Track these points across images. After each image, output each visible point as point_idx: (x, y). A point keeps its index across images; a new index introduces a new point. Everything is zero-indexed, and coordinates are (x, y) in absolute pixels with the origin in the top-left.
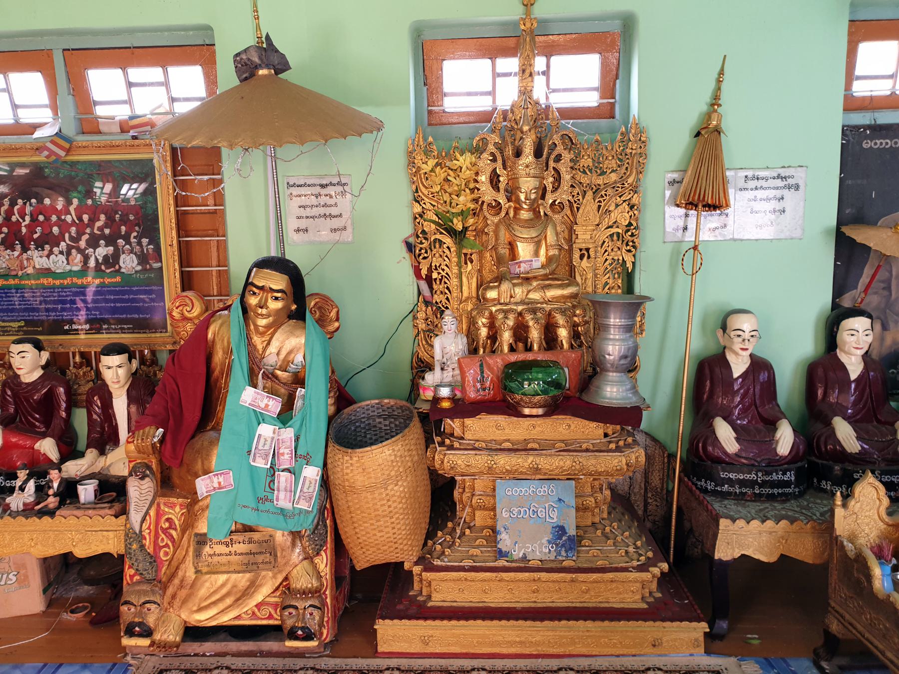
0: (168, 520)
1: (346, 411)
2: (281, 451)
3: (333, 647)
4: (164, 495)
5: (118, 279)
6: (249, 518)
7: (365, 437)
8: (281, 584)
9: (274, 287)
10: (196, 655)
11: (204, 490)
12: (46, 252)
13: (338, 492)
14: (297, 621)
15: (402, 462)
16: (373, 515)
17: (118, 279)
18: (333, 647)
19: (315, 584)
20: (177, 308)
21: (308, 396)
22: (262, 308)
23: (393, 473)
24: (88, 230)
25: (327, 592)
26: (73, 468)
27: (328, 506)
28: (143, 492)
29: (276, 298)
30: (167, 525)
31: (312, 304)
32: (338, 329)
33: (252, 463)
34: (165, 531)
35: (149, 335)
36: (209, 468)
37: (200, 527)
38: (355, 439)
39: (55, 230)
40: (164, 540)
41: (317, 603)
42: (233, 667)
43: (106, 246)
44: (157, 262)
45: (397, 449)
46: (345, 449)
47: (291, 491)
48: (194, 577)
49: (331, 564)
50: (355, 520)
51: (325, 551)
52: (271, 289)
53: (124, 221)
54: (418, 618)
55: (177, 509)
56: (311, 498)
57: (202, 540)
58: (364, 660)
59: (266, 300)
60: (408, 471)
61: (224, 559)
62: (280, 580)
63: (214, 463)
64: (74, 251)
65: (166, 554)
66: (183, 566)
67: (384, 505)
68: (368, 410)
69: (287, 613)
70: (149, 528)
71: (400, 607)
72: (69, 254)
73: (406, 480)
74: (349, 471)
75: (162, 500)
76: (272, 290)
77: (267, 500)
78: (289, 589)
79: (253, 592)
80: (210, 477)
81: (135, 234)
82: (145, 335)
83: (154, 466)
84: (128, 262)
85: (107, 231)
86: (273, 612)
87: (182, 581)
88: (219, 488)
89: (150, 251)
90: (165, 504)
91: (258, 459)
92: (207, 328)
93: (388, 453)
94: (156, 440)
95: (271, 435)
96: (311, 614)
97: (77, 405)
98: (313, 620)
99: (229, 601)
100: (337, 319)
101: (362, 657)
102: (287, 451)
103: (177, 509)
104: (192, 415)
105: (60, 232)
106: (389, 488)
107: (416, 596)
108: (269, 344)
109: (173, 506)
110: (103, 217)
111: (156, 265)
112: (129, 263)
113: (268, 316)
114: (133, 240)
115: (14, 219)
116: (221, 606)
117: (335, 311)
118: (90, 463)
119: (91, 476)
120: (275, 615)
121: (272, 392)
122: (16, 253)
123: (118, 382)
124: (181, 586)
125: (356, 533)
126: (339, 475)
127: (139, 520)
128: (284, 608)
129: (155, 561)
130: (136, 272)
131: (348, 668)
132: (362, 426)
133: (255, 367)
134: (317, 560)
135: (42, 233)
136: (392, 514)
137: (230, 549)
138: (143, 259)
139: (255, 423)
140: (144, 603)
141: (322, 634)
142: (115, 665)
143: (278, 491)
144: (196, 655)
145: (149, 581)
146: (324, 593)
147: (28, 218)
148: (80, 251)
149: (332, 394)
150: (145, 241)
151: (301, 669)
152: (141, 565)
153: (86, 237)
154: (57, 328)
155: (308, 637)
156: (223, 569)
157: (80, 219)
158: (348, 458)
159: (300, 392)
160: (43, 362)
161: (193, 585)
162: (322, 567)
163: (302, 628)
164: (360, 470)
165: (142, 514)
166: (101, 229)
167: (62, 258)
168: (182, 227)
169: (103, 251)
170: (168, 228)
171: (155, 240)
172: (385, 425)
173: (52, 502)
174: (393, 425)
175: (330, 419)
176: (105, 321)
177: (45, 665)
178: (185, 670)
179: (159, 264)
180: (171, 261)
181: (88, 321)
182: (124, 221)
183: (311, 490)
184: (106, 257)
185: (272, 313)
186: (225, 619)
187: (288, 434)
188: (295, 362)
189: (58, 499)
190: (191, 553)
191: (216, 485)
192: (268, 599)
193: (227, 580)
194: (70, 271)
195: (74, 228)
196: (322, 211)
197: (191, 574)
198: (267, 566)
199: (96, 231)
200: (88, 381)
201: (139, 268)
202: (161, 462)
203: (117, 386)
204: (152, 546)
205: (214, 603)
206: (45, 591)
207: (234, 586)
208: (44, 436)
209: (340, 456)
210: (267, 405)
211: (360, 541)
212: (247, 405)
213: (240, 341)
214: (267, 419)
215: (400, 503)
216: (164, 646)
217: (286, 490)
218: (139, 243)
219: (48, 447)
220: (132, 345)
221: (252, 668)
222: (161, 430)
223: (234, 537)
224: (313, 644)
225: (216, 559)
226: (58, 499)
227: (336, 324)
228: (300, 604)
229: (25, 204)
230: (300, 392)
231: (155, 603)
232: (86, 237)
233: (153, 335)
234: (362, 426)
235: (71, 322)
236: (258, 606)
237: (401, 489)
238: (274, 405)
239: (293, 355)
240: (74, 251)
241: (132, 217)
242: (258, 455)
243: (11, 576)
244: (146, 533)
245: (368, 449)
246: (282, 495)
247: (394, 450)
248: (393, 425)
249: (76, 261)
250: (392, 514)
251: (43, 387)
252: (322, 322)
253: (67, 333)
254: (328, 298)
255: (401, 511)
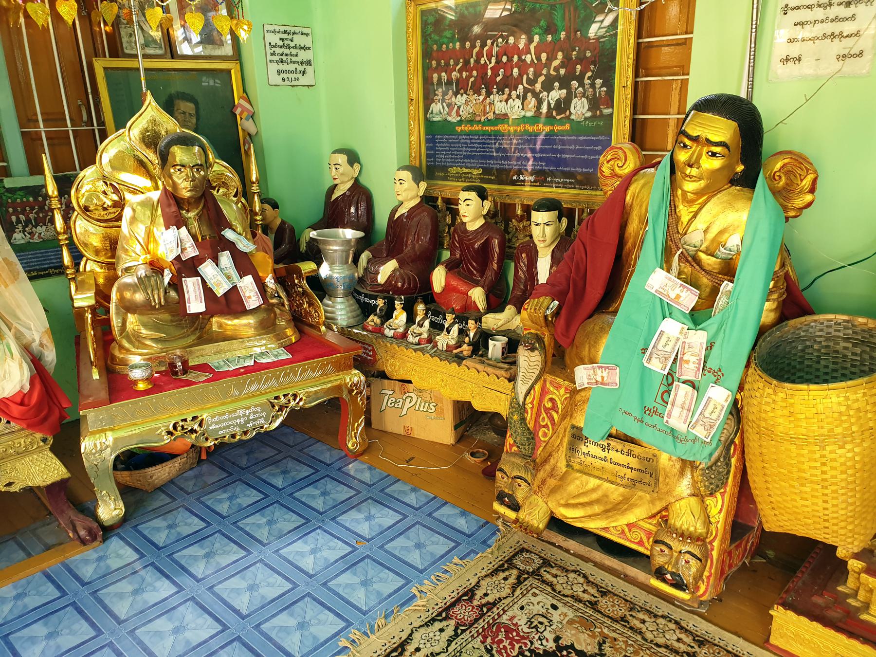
0: (552, 400)
1: (792, 322)
2: (686, 357)
3: (712, 609)
4: (552, 373)
5: (567, 127)
6: (632, 429)
7: (818, 362)
8: (660, 512)
9: (714, 138)
10: (560, 547)
11: (586, 381)
12: (505, 96)
13: (750, 430)
14: (669, 563)
15: (859, 418)
16: (795, 476)
17: (567, 127)
18: (712, 609)
19: (700, 529)
20: (608, 162)
21: (736, 293)
22: (691, 166)
23: (839, 430)
24: (544, 72)
25: (715, 544)
26: (492, 321)
27: (737, 440)
28: (532, 364)
29: (714, 154)
30: (549, 405)
31: (779, 165)
32: (809, 204)
33: (646, 364)
34: (547, 410)
35: (589, 192)
36: (595, 357)
37: (578, 419)
38: (801, 363)
39: (516, 71)
40: (545, 420)
41: (697, 552)
42: (591, 579)
43: (560, 89)
44: (608, 108)
45: (853, 397)
46: (769, 379)
47: (689, 410)
48: (564, 469)
49: (728, 512)
50: (768, 472)
51: (723, 495)
52: (707, 140)
53: (581, 60)
54: (839, 629)
55: (562, 391)
56: (711, 427)
57: (578, 436)
58: (746, 644)
59: (699, 157)
60: (867, 434)
61: (598, 463)
62: (658, 508)
63: (601, 352)
64: (529, 95)
65: (545, 435)
66: (555, 455)
67: (815, 468)
68: (829, 327)
69: (658, 549)
70: (532, 403)
71: (818, 600)
72: (524, 98)
73: (858, 445)
74: (768, 409)
75: (549, 378)
76: (709, 142)
77: (656, 412)
78: (666, 521)
79: (626, 510)
80: (593, 368)
81: (589, 74)
82: (586, 192)
83: (546, 340)
84: (579, 107)
85: (562, 71)
86: (645, 539)
87: (553, 469)
88: (602, 384)
89: (603, 93)
90: (551, 383)
91: (654, 360)
92: (627, 189)
93: (835, 399)
94: (549, 312)
95: (677, 335)
96: (687, 562)
97: (511, 257)
98: (689, 570)
99: (597, 509)
100: (812, 190)
101: (746, 639)
102: (693, 359)
103: (562, 391)
104: (595, 292)
105: (520, 74)
106: (828, 448)
107: (847, 596)
108: (695, 216)
109: (558, 387)
110: (560, 55)
111: (607, 111)
112: (580, 108)
113: (700, 179)
114: (587, 81)
115: (482, 62)
116: (589, 511)
117: (811, 177)
118: (507, 320)
119: (504, 333)
120: (646, 544)
121: (693, 282)
122: (481, 98)
123: (544, 241)
124: (551, 475)
125: (767, 488)
126: (754, 409)
127: (524, 392)
128: (656, 542)
129: (533, 438)
130: (586, 119)
131: (722, 644)
132: (816, 347)
133: (673, 246)
134: (709, 501)
135: (504, 75)
136: (826, 484)
137: (605, 454)
138: (594, 104)
139: (660, 316)
140: (515, 477)
141: (698, 588)
142: (487, 523)
143: (673, 405)
144: (560, 547)
145: (524, 457)
146: (711, 543)
147: (493, 60)
148: (536, 95)
149: (775, 296)
150: (599, 82)
151: (663, 617)
152: (518, 438)
153: (542, 78)
154: (504, 177)
155: (679, 585)
156: (596, 473)
157: (539, 58)
158: (770, 391)
159: (726, 286)
160: (485, 212)
161: (563, 478)
162: (714, 511)
163: (672, 574)
164: (786, 412)
165: (527, 387)
166: (557, 69)
167: (518, 102)
168: (640, 64)
169: (557, 94)
170: (625, 65)
171: (609, 84)
172: (853, 354)
173: (466, 349)
174: (867, 357)
175: (762, 331)
176: (552, 174)
177: (435, 498)
178: (544, 559)
179: (610, 110)
180: (623, 106)
181: (534, 172)
182: (581, 60)
183: (714, 416)
184: (558, 102)
185: (705, 174)
186: (592, 525)
187: (699, 338)
188: (728, 245)
189: (471, 347)
190: (565, 444)
191: (599, 379)
192: (641, 523)
193: (599, 487)
194: (524, 117)
195: (532, 69)
196: (829, 28)
197: (562, 466)
198: (646, 488)
199: (552, 73)
200: (526, 236)
201: (589, 114)
202: (553, 337)
203: (542, 245)
204: (533, 422)
205: (583, 505)
206: (456, 427)
207: (606, 496)
208: (476, 284)
209: (761, 385)
210: (678, 297)
211: (772, 499)
212: (653, 291)
213: (659, 208)
214: (676, 313)
215: (842, 473)
216: (526, 528)
217: (683, 407)
218: (593, 85)
219: (477, 295)
220: (567, 203)
221: (610, 589)
222: (556, 302)
223: (612, 443)
224: (684, 596)
225: (589, 459)
226: (471, 347)
227: (809, 198)
228: (676, 545)
229: (492, 44)
230: (726, 286)
231: (526, 481)
232: (542, 78)
233: (594, 193)
234: (816, 347)
235: (520, 172)
236: (630, 526)
237: (850, 455)
238: (689, 298)
239: (727, 235)
240: (529, 95)
241: (588, 54)
242: (655, 356)
243: (431, 406)
244: (529, 407)
245: (804, 387)
246: (676, 411)
247: (847, 398)
248: (867, 357)
249: (530, 106)
250: (826, 484)
251: (482, 237)
252: (782, 195)
253: (514, 183)
254: (805, 159)
255: (843, 484)
